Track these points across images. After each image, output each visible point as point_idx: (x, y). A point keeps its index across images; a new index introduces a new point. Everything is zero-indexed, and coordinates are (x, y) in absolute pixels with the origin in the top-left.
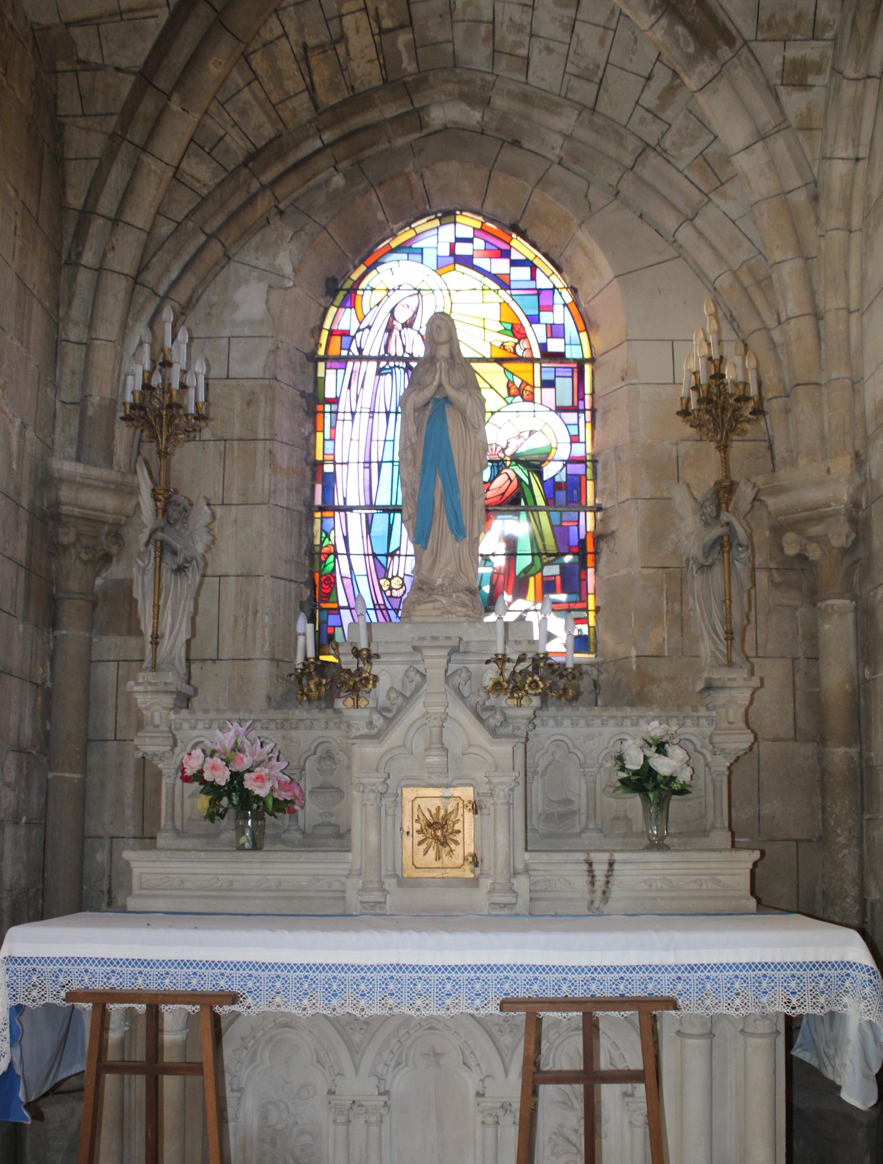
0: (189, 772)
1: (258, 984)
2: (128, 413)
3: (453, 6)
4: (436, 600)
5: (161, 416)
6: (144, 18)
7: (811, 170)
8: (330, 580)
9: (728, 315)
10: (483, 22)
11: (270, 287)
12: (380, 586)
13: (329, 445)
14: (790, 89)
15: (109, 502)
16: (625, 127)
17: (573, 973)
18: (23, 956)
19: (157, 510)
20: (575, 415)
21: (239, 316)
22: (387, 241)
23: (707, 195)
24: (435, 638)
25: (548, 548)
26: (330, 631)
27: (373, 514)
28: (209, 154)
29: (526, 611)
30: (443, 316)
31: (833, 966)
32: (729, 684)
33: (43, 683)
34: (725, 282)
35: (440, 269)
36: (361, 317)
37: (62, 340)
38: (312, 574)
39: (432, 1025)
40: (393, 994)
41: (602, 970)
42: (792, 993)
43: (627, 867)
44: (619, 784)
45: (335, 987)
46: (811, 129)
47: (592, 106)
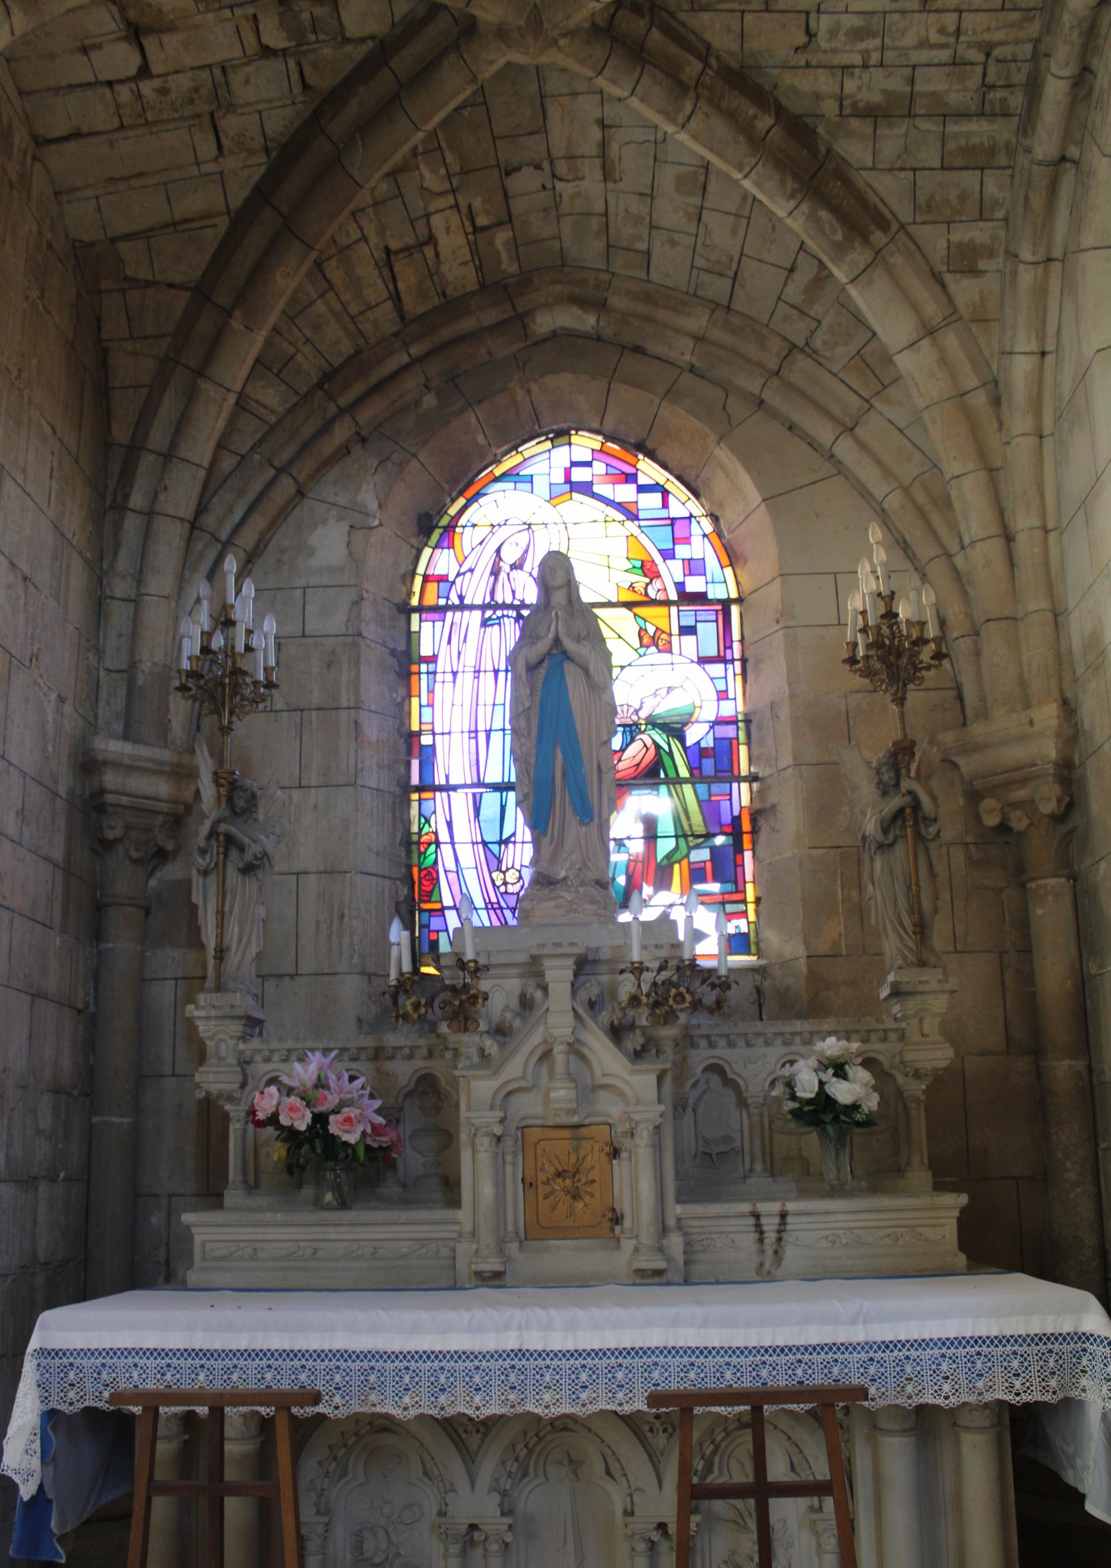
0: (261, 1116)
1: (347, 1378)
2: (184, 681)
3: (558, 199)
4: (559, 897)
5: (223, 685)
6: (201, 228)
7: (989, 366)
8: (431, 875)
9: (901, 541)
10: (595, 215)
11: (351, 527)
12: (493, 881)
13: (427, 712)
14: (958, 275)
15: (163, 788)
16: (767, 326)
17: (738, 1357)
18: (57, 1347)
19: (219, 797)
20: (722, 666)
21: (315, 562)
22: (490, 469)
23: (867, 401)
24: (557, 945)
25: (695, 828)
26: (433, 936)
27: (481, 794)
28: (277, 375)
29: (671, 906)
30: (558, 556)
31: (1064, 1339)
32: (920, 988)
33: (86, 1008)
34: (894, 502)
35: (553, 498)
36: (461, 559)
37: (107, 597)
38: (409, 867)
39: (564, 1424)
40: (514, 1388)
41: (774, 1351)
42: (1014, 1375)
43: (804, 1219)
44: (790, 1116)
45: (443, 1380)
46: (986, 321)
47: (726, 303)
